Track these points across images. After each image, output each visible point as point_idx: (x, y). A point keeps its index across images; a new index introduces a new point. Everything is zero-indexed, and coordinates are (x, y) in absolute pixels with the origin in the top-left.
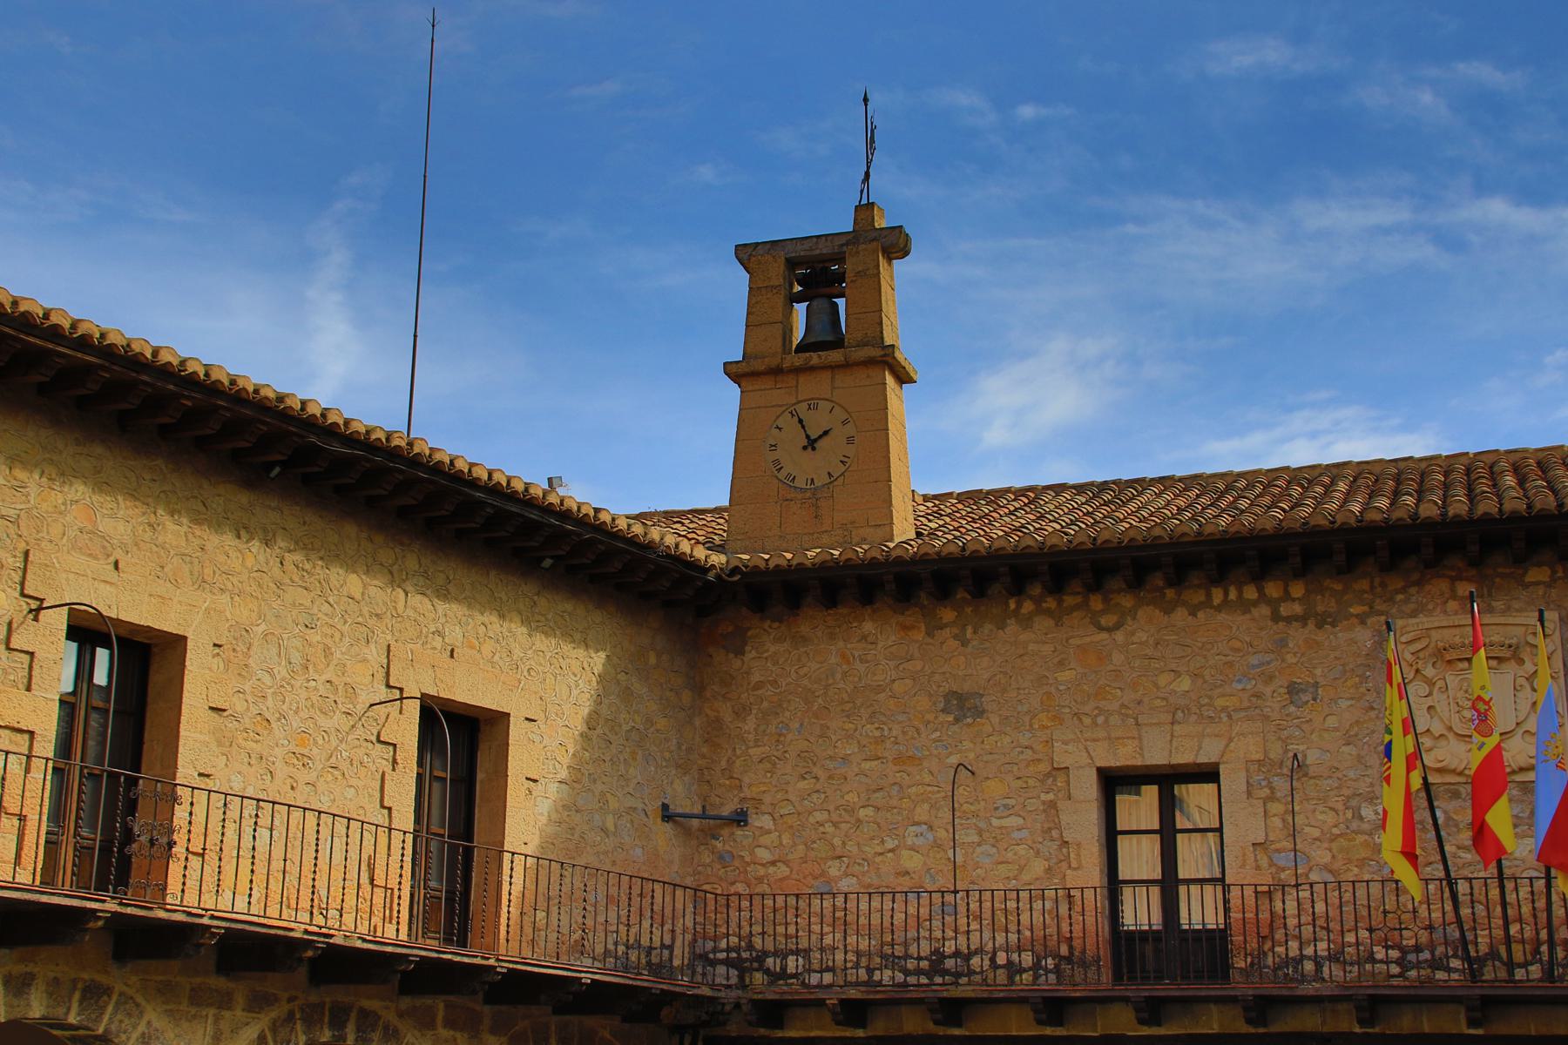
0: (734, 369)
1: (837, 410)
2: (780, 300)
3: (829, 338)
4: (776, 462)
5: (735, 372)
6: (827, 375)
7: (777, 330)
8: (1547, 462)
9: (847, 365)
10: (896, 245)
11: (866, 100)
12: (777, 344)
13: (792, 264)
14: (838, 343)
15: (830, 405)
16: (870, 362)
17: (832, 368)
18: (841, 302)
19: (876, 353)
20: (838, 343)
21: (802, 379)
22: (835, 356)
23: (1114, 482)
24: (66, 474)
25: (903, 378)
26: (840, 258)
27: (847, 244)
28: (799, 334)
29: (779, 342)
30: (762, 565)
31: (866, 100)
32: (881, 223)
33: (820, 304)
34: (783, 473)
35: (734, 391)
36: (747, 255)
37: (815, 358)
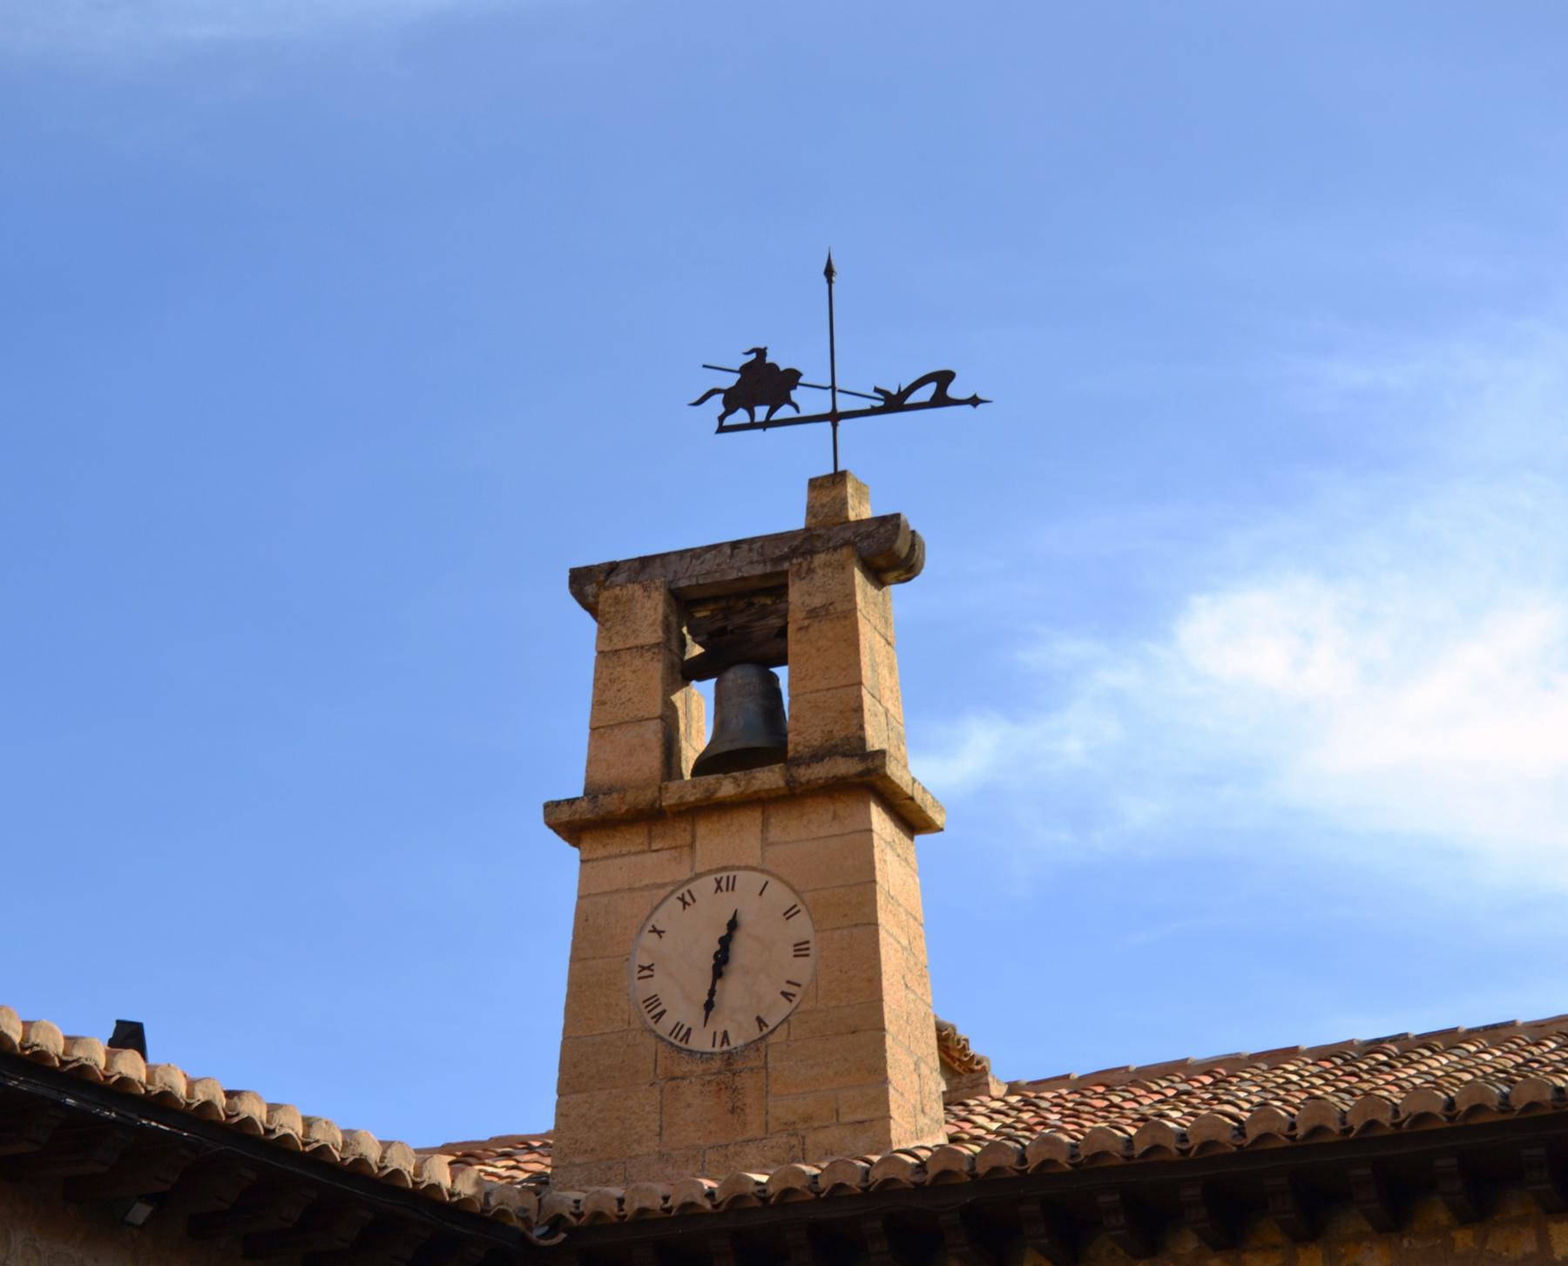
0: (564, 815)
1: (775, 887)
2: (655, 670)
3: (758, 742)
4: (652, 1001)
5: (573, 824)
6: (750, 821)
7: (652, 733)
8: (1567, 1031)
9: (793, 796)
10: (889, 554)
11: (829, 272)
12: (652, 761)
13: (683, 603)
14: (773, 750)
15: (759, 879)
16: (837, 789)
17: (762, 802)
18: (782, 672)
19: (845, 767)
20: (773, 750)
21: (702, 829)
22: (769, 778)
23: (1393, 1040)
24: (897, 781)
25: (912, 821)
26: (776, 588)
27: (794, 552)
28: (697, 736)
29: (657, 753)
30: (611, 1209)
31: (829, 272)
32: (861, 510)
33: (742, 676)
34: (667, 1024)
35: (566, 858)
36: (588, 585)
37: (727, 788)
